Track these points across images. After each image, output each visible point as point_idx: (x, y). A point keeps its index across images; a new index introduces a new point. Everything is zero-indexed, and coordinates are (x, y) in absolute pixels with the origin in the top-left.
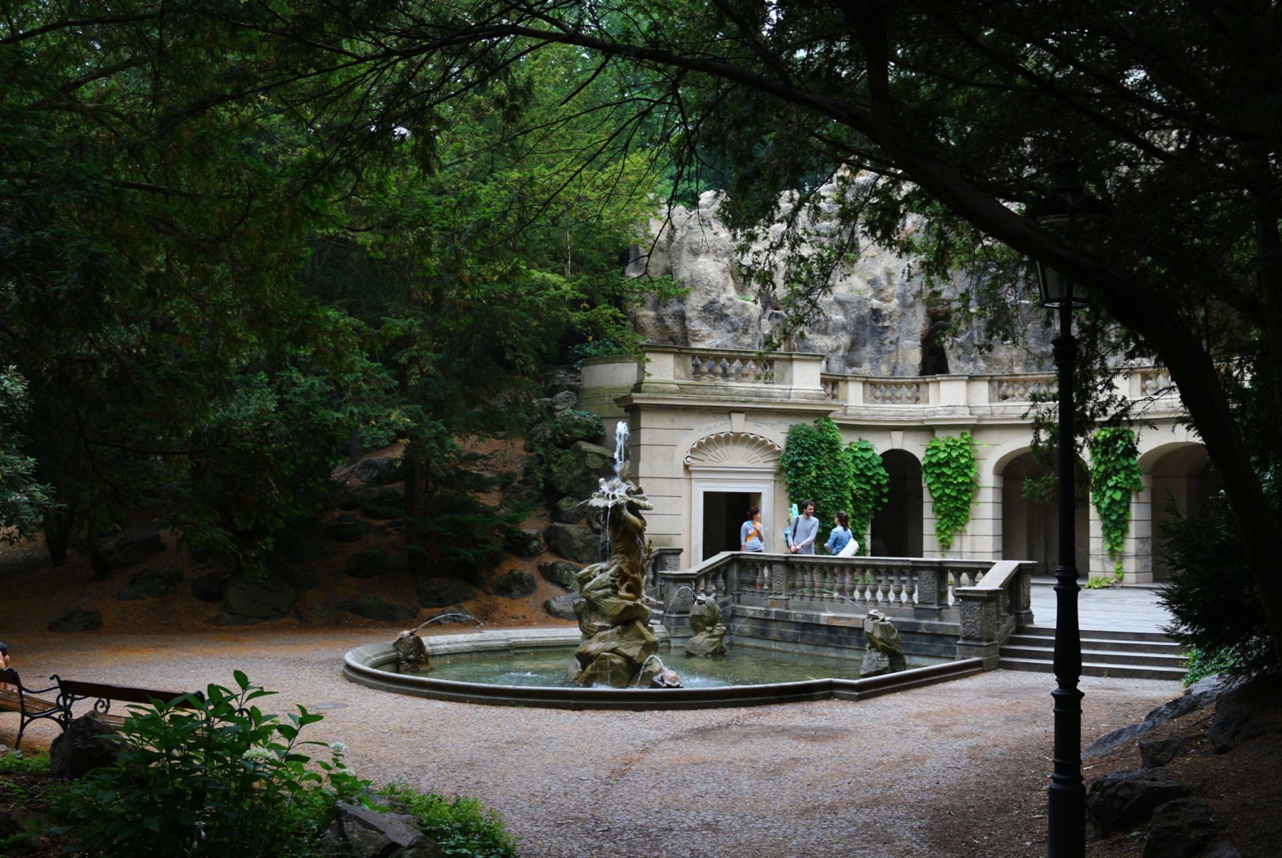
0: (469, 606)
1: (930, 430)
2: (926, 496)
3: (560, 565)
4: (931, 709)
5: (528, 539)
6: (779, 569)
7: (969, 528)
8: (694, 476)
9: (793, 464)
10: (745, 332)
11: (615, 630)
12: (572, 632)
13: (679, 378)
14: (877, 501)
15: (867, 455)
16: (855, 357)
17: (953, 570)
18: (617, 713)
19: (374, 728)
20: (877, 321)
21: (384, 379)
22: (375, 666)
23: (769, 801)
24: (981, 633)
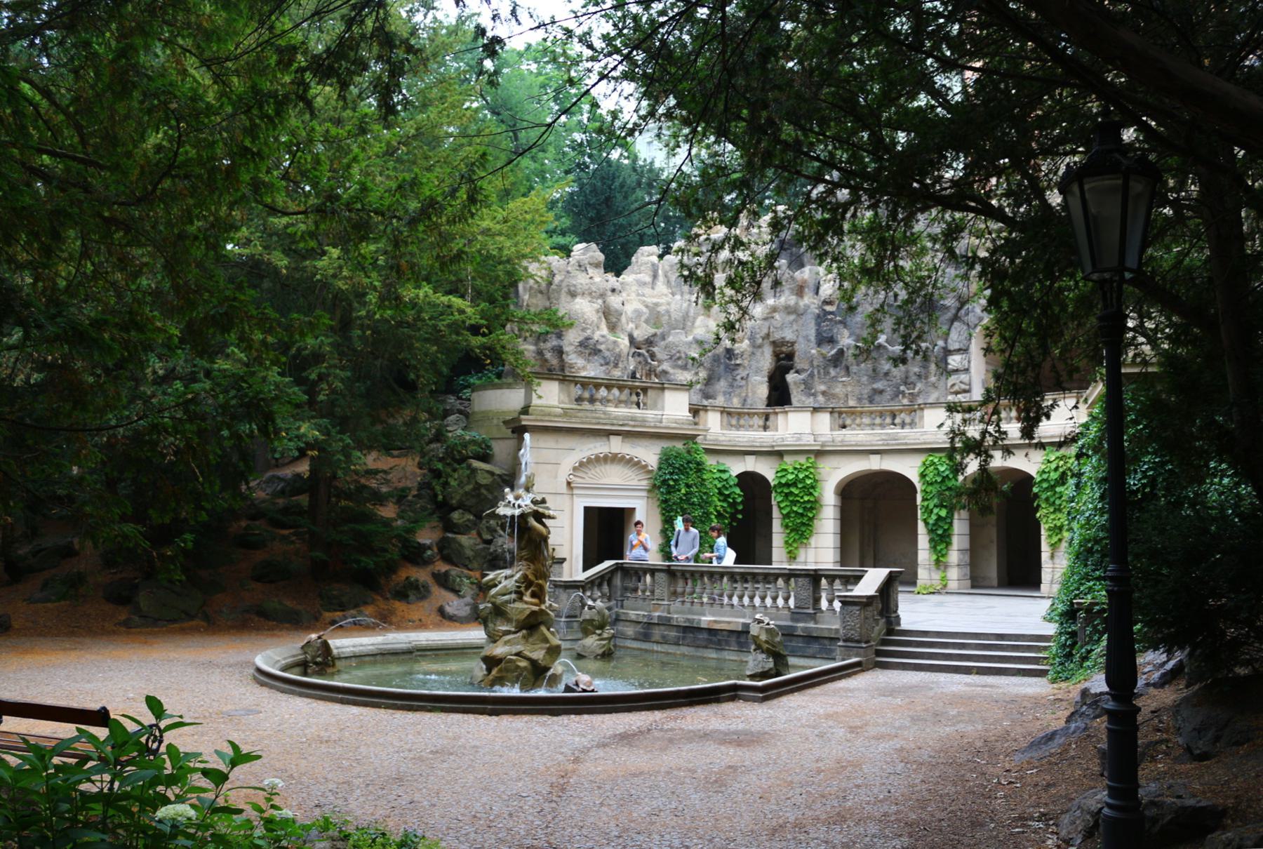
0: (369, 610)
1: (779, 454)
2: (776, 513)
3: (453, 573)
4: (835, 709)
5: (424, 548)
6: (661, 577)
7: (813, 541)
8: (575, 492)
9: (664, 482)
10: (616, 366)
11: (520, 634)
12: (476, 635)
13: (563, 402)
14: (733, 517)
15: (725, 476)
16: (710, 390)
17: (827, 577)
18: (535, 718)
19: (291, 737)
20: (730, 359)
21: (294, 393)
22: (284, 670)
23: (729, 819)
24: (860, 635)
